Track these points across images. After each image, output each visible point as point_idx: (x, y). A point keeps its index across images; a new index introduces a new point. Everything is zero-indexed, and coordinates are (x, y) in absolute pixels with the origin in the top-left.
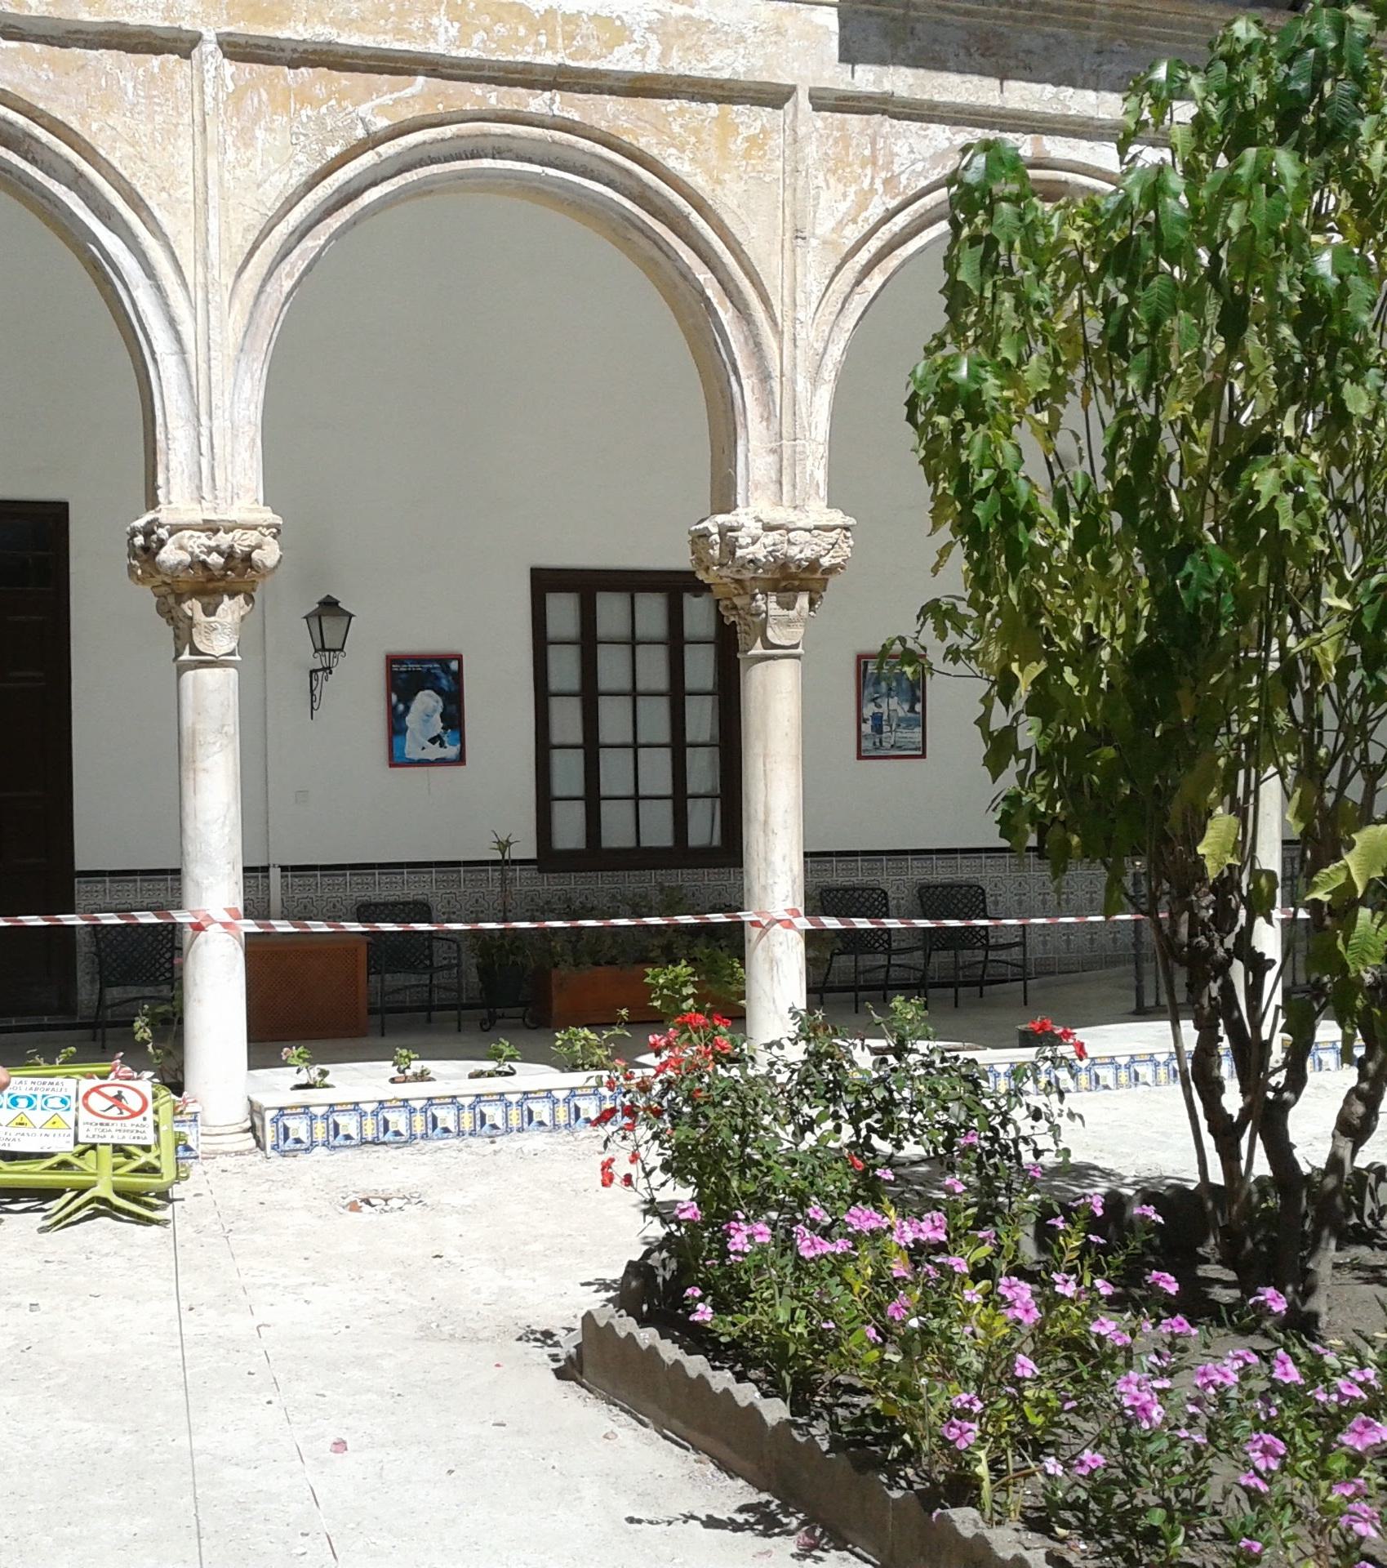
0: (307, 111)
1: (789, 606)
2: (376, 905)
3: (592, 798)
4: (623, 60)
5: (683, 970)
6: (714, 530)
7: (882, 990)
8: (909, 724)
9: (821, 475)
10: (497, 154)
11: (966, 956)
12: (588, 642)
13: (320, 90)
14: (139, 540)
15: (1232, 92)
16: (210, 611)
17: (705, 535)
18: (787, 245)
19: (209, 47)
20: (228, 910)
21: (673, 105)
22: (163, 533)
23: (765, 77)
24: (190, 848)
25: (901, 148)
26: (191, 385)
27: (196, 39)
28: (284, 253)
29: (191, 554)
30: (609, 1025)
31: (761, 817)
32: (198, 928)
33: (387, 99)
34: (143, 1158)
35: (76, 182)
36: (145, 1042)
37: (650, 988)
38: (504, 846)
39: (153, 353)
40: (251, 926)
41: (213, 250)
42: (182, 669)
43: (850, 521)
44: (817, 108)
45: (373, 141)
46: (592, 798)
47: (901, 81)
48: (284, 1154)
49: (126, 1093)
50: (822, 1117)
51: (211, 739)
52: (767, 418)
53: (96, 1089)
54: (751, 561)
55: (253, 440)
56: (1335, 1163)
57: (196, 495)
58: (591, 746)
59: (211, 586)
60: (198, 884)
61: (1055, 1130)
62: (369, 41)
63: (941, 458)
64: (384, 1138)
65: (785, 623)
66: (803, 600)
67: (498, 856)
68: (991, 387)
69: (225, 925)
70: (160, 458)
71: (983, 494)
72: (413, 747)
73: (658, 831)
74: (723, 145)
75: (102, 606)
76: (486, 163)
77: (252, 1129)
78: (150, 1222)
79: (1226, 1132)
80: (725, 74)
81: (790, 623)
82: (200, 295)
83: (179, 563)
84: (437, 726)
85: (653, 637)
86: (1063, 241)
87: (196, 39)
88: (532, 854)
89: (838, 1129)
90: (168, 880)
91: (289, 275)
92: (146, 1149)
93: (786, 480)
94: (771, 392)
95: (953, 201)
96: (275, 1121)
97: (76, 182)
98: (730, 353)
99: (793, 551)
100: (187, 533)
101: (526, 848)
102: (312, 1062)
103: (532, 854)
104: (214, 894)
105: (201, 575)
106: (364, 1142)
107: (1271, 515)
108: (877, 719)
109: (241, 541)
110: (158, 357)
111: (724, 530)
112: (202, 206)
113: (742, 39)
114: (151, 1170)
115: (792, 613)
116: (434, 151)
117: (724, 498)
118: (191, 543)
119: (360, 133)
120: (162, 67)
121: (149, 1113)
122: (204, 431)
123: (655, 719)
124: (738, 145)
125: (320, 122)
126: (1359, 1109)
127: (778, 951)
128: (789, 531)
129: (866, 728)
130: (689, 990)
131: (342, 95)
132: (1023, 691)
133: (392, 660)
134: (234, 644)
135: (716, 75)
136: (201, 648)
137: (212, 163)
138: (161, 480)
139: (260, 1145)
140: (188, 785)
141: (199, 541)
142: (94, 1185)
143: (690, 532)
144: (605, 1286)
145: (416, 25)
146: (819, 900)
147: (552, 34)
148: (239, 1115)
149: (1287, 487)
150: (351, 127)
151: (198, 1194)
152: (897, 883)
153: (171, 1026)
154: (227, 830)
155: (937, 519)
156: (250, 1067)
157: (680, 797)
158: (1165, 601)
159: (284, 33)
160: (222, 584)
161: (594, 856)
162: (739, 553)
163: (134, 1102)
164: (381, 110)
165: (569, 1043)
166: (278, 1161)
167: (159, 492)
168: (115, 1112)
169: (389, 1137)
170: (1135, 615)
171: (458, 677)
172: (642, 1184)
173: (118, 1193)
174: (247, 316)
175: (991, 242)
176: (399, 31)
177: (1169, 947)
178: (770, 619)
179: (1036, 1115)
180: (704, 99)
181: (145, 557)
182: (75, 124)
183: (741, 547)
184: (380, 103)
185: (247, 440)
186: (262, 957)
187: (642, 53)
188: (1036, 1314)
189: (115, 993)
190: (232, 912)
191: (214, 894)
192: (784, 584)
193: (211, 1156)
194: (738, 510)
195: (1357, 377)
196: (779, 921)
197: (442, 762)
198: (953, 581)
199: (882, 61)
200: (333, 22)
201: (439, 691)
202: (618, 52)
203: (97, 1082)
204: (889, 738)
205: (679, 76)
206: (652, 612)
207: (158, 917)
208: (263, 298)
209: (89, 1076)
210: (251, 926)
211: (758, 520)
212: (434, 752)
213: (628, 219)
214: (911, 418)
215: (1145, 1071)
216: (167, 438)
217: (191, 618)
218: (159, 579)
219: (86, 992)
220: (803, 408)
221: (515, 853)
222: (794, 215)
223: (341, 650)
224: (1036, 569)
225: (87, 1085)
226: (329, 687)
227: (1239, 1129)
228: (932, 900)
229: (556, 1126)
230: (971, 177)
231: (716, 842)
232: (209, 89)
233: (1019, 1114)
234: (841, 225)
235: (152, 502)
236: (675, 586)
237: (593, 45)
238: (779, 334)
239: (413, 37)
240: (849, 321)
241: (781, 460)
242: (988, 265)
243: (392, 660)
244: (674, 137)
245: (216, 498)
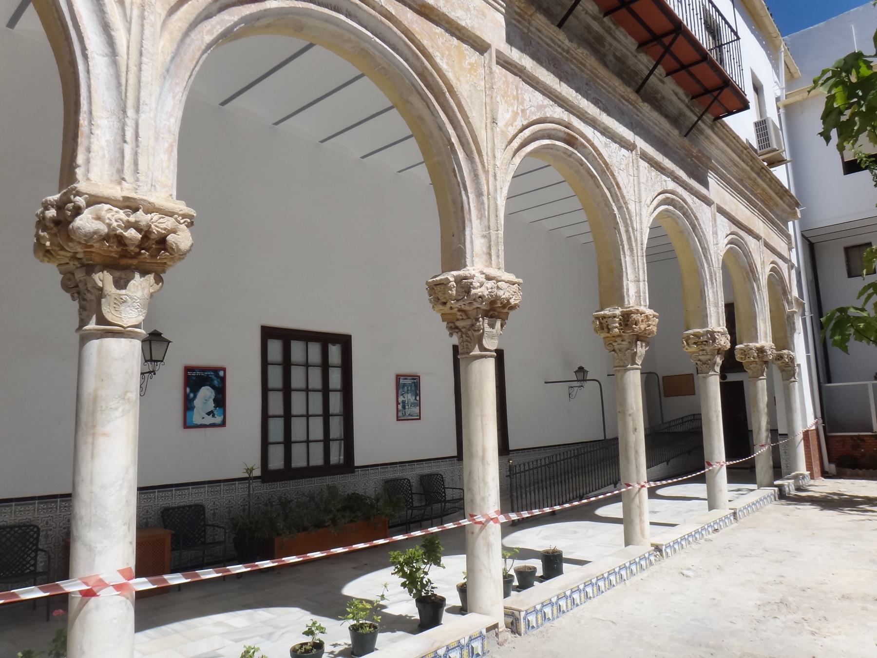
2: (173, 509)
3: (288, 442)
6: (452, 279)
12: (287, 364)
14: (52, 213)
16: (121, 284)
18: (489, 125)
20: (122, 572)
21: (439, 30)
22: (81, 201)
26: (119, 84)
29: (109, 225)
31: (480, 453)
32: (89, 594)
39: (84, 49)
40: (144, 584)
42: (85, 338)
43: (521, 281)
46: (288, 442)
51: (113, 404)
52: (481, 217)
54: (480, 297)
55: (171, 146)
57: (116, 177)
58: (287, 416)
59: (124, 262)
60: (90, 549)
67: (247, 475)
69: (118, 587)
70: (82, 141)
72: (197, 417)
73: (317, 460)
80: (463, 23)
82: (136, 13)
83: (95, 233)
84: (211, 405)
91: (210, 32)
93: (493, 252)
94: (483, 203)
98: (463, 177)
99: (500, 293)
100: (107, 207)
101: (257, 472)
108: (404, 402)
109: (159, 224)
110: (89, 53)
111: (459, 280)
115: (494, 331)
118: (109, 215)
122: (130, 122)
123: (316, 400)
128: (498, 281)
129: (400, 407)
133: (188, 369)
134: (141, 318)
135: (460, 22)
136: (109, 317)
138: (80, 159)
140: (85, 451)
141: (117, 216)
143: (427, 283)
154: (124, 492)
157: (327, 441)
160: (135, 262)
161: (289, 473)
162: (473, 291)
167: (78, 170)
171: (223, 380)
174: (175, 46)
178: (485, 335)
181: (55, 230)
183: (474, 288)
185: (166, 145)
192: (491, 313)
194: (468, 268)
196: (492, 519)
197: (213, 425)
201: (213, 387)
204: (409, 410)
205: (443, 13)
206: (315, 350)
207: (44, 590)
208: (188, 40)
211: (482, 273)
212: (209, 420)
213: (414, 85)
216: (90, 123)
217: (101, 289)
222: (492, 110)
223: (162, 361)
231: (342, 462)
238: (486, 172)
241: (490, 241)
243: (188, 369)
245: (137, 180)
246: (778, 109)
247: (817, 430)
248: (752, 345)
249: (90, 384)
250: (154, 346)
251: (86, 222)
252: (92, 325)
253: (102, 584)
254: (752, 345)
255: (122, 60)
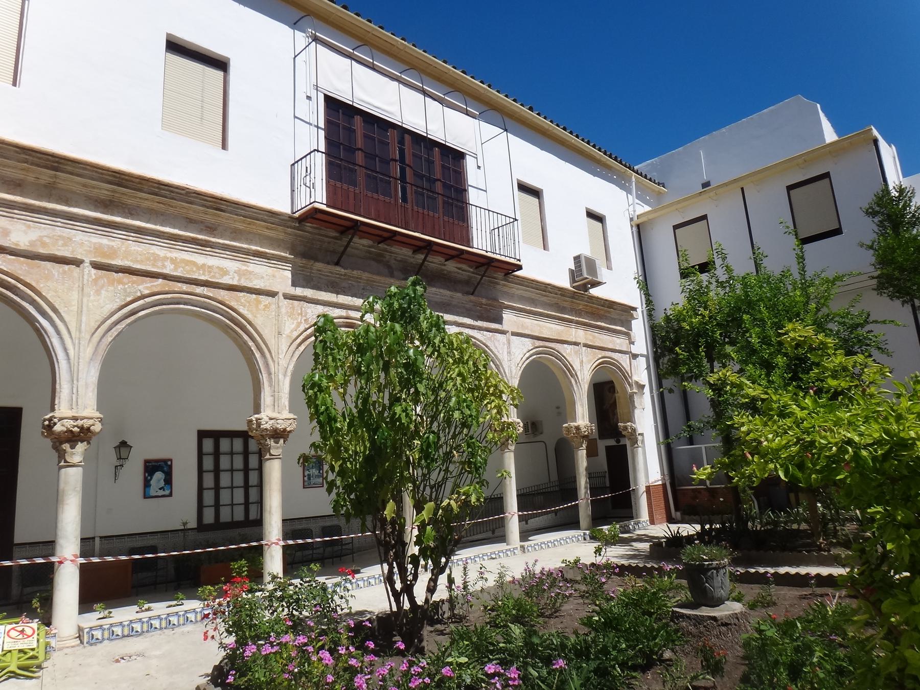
0: (120, 287)
1: (277, 443)
3: (217, 505)
4: (226, 280)
5: (243, 562)
7: (307, 562)
8: (318, 476)
9: (287, 403)
10: (185, 304)
11: (336, 548)
12: (217, 454)
13: (125, 280)
14: (47, 423)
15: (390, 305)
16: (73, 447)
17: (251, 421)
19: (87, 264)
21: (242, 294)
22: (56, 420)
23: (269, 289)
24: (59, 533)
25: (309, 311)
27: (82, 262)
28: (110, 329)
30: (217, 584)
32: (61, 563)
33: (149, 285)
34: (31, 653)
35: (33, 302)
36: (36, 608)
37: (232, 569)
38: (185, 524)
40: (82, 560)
41: (83, 325)
42: (61, 468)
44: (285, 298)
45: (143, 297)
46: (217, 505)
47: (309, 293)
48: (91, 645)
49: (26, 629)
50: (278, 607)
52: (271, 385)
53: (13, 629)
56: (427, 601)
58: (217, 488)
60: (62, 547)
61: (347, 601)
62: (143, 267)
63: (311, 402)
64: (132, 633)
65: (276, 448)
66: (282, 441)
68: (325, 382)
71: (322, 413)
72: (152, 492)
74: (257, 307)
75: (32, 446)
76: (182, 306)
77: (79, 637)
78: (32, 678)
79: (397, 595)
81: (278, 448)
84: (162, 483)
85: (233, 452)
86: (346, 342)
87: (82, 262)
88: (195, 526)
89: (283, 610)
90: (49, 546)
92: (33, 650)
95: (316, 330)
96: (88, 633)
97: (33, 302)
99: (278, 426)
101: (193, 524)
102: (105, 609)
103: (195, 526)
104: (69, 549)
105: (70, 435)
106: (124, 636)
107: (399, 419)
109: (86, 423)
111: (257, 419)
112: (80, 312)
113: (263, 278)
114: (34, 657)
116: (164, 302)
117: (257, 410)
119: (139, 294)
120: (69, 269)
121: (35, 636)
122: (75, 386)
124: (261, 306)
125: (125, 290)
126: (432, 584)
127: (274, 553)
129: (306, 479)
130: (246, 569)
131: (133, 282)
132: (337, 469)
133: (147, 462)
137: (85, 300)
138: (56, 402)
139: (82, 642)
140: (60, 511)
142: (8, 666)
144: (207, 675)
145: (160, 264)
146: (286, 535)
147: (204, 271)
148: (73, 632)
149: (403, 411)
150: (136, 292)
151: (54, 665)
152: (315, 527)
153: (47, 602)
155: (311, 419)
156: (80, 613)
158: (373, 442)
159: (113, 262)
161: (218, 525)
163: (28, 631)
164: (147, 288)
165: (203, 592)
166: (89, 648)
168: (21, 636)
169: (134, 633)
170: (365, 447)
171: (170, 467)
172: (217, 637)
173: (19, 668)
175: (325, 342)
176: (153, 265)
177: (379, 542)
179: (342, 597)
180: (252, 293)
182: (34, 284)
184: (146, 286)
186: (85, 571)
187: (233, 279)
188: (332, 661)
189: (28, 590)
190: (76, 556)
191: (69, 549)
193: (61, 649)
195: (420, 382)
198: (317, 438)
199: (303, 287)
200: (131, 261)
201: (163, 472)
202: (225, 278)
203: (14, 625)
204: (313, 481)
206: (238, 444)
209: (11, 624)
210: (82, 560)
212: (161, 493)
214: (303, 390)
215: (372, 581)
218: (53, 437)
219: (15, 590)
220: (281, 384)
221: (189, 526)
224: (338, 434)
225: (9, 627)
226: (122, 472)
227: (400, 594)
228: (326, 531)
229: (197, 621)
230: (320, 324)
232: (86, 277)
233: (336, 598)
234: (292, 331)
235: (53, 409)
236: (244, 435)
237: (217, 275)
238: (274, 361)
239: (158, 267)
240: (295, 359)
242: (325, 348)
243: (147, 462)
244: (243, 304)
246: (632, 226)
247: (664, 485)
248: (572, 424)
249: (62, 485)
250: (122, 450)
251: (58, 428)
252: (62, 464)
253: (66, 559)
254: (572, 424)
255: (72, 361)
